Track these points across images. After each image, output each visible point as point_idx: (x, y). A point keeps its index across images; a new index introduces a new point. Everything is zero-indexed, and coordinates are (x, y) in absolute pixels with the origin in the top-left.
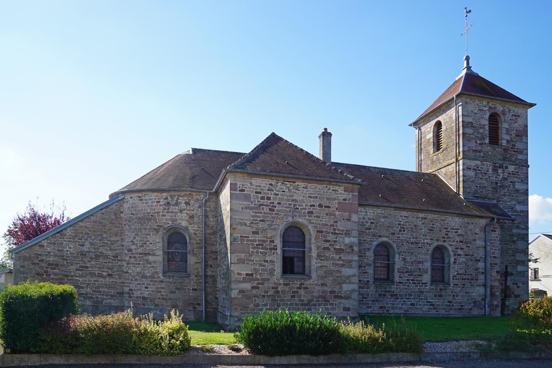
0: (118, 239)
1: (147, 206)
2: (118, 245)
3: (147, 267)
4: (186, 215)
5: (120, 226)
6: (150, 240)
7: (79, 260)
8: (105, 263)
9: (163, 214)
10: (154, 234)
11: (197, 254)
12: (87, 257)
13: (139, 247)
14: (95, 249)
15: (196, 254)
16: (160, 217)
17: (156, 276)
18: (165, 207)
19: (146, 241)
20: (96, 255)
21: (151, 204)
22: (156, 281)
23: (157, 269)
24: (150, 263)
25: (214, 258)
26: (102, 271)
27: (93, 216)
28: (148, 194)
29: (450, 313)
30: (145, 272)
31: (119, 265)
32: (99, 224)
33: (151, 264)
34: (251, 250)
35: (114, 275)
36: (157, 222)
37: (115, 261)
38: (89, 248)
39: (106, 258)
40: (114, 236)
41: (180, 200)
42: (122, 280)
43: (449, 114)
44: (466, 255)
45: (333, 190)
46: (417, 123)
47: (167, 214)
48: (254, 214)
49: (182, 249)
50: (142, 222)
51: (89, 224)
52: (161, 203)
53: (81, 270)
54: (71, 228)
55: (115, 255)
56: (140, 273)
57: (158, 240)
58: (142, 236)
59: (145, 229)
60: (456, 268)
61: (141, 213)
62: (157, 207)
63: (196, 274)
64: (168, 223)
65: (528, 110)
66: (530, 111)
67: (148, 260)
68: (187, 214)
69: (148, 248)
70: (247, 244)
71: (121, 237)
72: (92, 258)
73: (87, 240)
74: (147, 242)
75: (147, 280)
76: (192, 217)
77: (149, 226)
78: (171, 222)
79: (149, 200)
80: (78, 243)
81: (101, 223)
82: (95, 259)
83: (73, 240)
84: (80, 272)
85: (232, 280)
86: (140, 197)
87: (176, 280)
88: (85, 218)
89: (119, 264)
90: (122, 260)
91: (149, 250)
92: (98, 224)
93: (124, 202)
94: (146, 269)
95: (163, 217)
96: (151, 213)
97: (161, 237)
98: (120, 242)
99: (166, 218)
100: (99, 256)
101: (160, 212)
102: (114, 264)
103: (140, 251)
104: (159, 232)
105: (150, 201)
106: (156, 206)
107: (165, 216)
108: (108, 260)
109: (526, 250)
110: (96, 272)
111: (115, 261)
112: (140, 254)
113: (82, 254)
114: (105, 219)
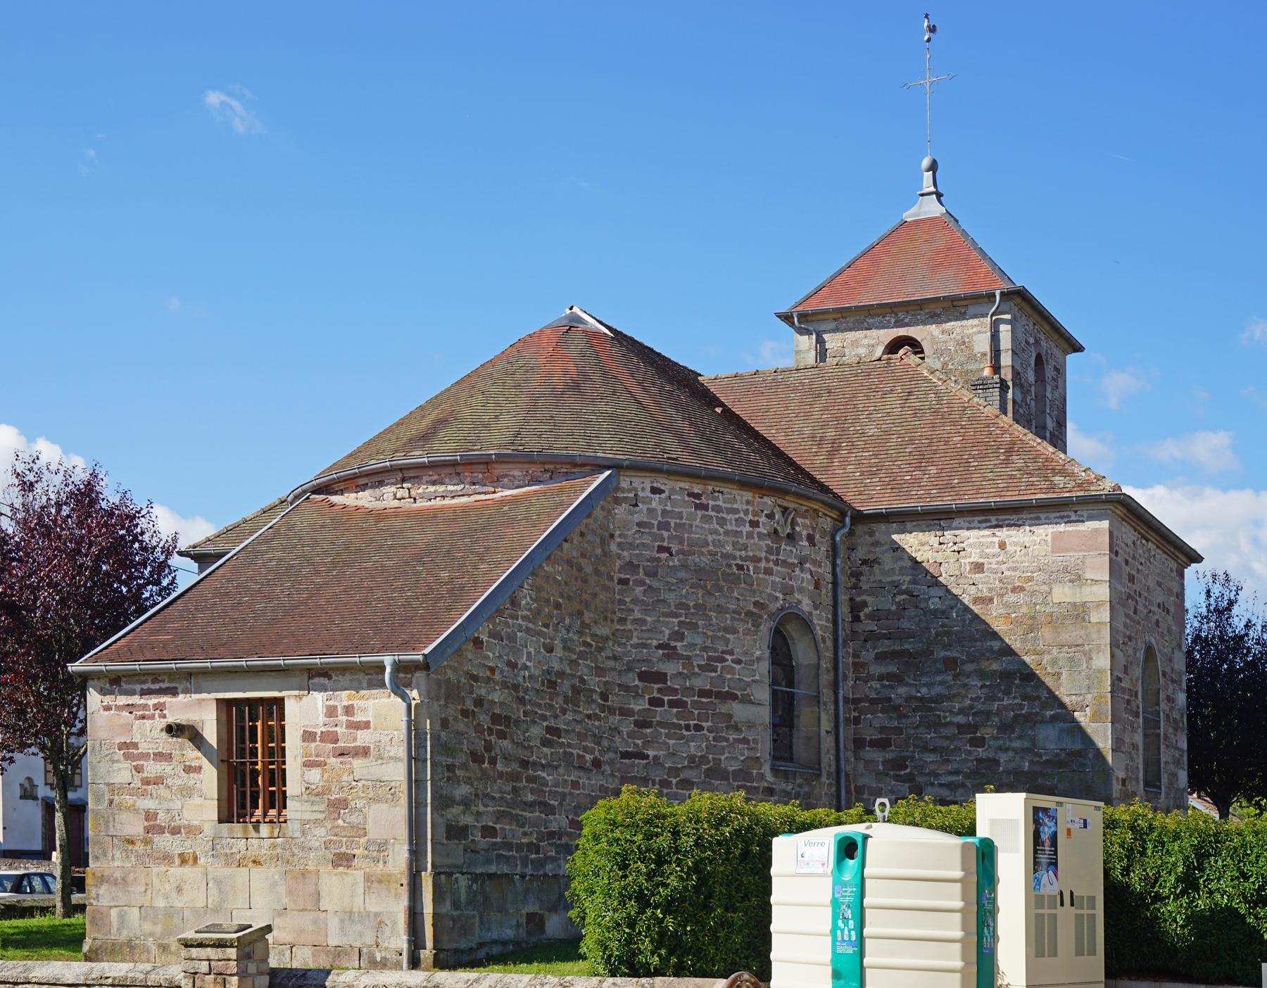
1: (722, 530)
3: (727, 740)
6: (735, 652)
10: (747, 632)
13: (696, 670)
16: (760, 576)
19: (723, 652)
24: (736, 728)
28: (725, 490)
30: (723, 758)
36: (754, 591)
43: (958, 330)
46: (809, 318)
52: (762, 530)
57: (758, 653)
58: (710, 633)
59: (720, 609)
61: (702, 554)
62: (752, 541)
67: (730, 716)
69: (729, 676)
77: (734, 601)
78: (781, 596)
86: (698, 496)
91: (732, 684)
94: (723, 748)
96: (735, 558)
97: (767, 644)
103: (701, 682)
105: (730, 516)
106: (750, 536)
112: (702, 693)
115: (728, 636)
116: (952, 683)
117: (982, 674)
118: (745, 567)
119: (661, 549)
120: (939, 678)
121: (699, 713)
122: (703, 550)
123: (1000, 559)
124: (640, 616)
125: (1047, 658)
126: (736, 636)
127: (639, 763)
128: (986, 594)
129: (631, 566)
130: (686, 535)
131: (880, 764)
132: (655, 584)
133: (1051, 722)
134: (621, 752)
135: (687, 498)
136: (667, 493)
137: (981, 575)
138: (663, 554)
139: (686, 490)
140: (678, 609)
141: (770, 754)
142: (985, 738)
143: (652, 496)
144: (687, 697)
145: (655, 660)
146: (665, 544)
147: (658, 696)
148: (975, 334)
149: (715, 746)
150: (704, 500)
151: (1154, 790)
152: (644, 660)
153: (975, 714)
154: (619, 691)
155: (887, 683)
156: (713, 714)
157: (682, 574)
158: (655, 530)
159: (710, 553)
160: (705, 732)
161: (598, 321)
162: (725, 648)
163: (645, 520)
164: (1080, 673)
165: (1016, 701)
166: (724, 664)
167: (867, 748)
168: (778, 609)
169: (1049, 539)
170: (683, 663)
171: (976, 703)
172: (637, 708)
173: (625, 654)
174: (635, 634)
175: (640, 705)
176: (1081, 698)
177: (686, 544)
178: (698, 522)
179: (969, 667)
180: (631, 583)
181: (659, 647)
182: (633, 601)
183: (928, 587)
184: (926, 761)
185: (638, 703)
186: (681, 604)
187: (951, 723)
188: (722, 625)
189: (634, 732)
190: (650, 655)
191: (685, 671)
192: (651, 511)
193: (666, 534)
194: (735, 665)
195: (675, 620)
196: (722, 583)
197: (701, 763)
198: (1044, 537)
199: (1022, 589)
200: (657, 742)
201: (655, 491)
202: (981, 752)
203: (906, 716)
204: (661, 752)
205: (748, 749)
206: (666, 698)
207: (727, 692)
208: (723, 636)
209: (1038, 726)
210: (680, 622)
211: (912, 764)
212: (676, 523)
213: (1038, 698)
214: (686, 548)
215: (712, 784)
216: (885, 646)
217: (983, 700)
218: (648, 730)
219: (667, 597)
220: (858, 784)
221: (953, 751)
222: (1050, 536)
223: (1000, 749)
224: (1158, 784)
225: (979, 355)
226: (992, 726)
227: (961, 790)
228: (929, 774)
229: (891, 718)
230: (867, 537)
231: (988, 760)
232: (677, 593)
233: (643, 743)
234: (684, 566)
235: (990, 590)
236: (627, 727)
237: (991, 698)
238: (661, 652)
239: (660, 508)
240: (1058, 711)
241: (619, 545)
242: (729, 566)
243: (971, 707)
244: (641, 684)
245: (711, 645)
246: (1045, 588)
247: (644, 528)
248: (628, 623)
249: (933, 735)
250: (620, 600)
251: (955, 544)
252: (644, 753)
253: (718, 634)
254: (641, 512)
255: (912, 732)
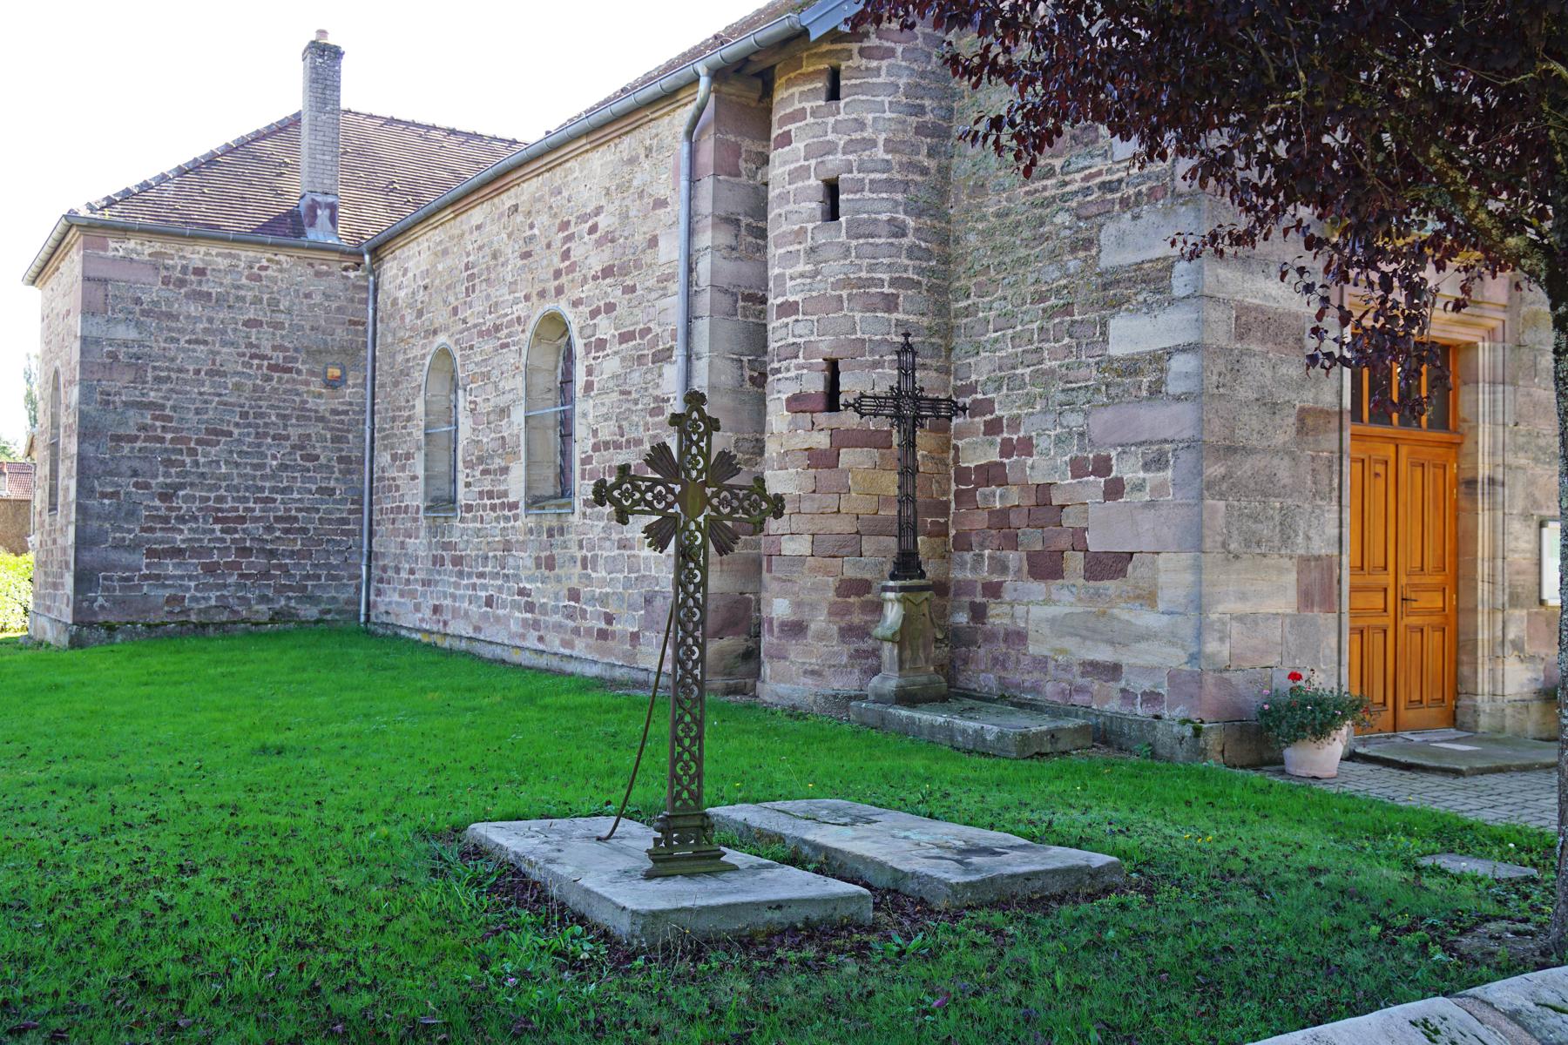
29: (575, 654)
44: (625, 338)
45: (873, 143)
60: (591, 417)
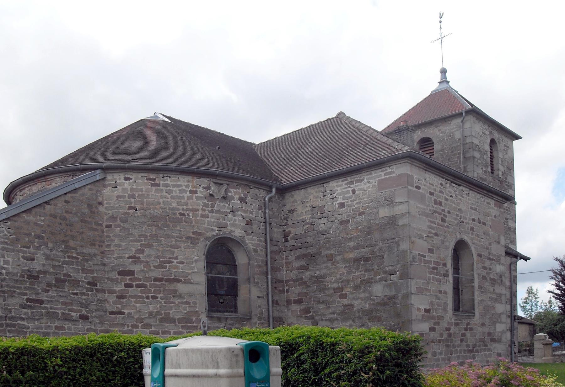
0: (96, 251)
1: (169, 196)
2: (96, 262)
3: (174, 303)
4: (241, 218)
5: (99, 228)
6: (179, 257)
7: (25, 288)
8: (74, 294)
9: (204, 213)
11: (258, 282)
12: (40, 282)
13: (152, 268)
14: (54, 267)
15: (258, 283)
16: (198, 218)
17: (194, 318)
18: (206, 201)
20: (57, 280)
21: (179, 195)
22: (194, 326)
23: (196, 307)
24: (180, 296)
25: (280, 291)
26: (69, 310)
27: (49, 204)
30: (171, 312)
31: (98, 300)
32: (61, 221)
33: (184, 298)
34: (428, 275)
35: (91, 317)
36: (193, 226)
37: (93, 291)
38: (43, 265)
39: (76, 285)
40: (89, 245)
41: (231, 192)
42: (106, 326)
47: (210, 214)
48: (429, 224)
49: (228, 274)
50: (160, 224)
51: (43, 218)
52: (199, 195)
53: (30, 307)
54: (8, 223)
55: (91, 280)
56: (159, 313)
57: (196, 258)
58: (161, 249)
59: (168, 236)
62: (192, 201)
63: (259, 315)
64: (213, 230)
65: (514, 142)
66: (515, 142)
67: (176, 291)
68: (243, 217)
70: (424, 265)
71: (101, 248)
72: (49, 285)
73: (38, 248)
74: (173, 260)
75: (176, 325)
76: (249, 223)
78: (217, 229)
79: (174, 186)
80: (21, 254)
81: (65, 219)
82: (55, 286)
83: (12, 247)
84: (29, 311)
85: (413, 318)
86: (153, 180)
87: (230, 324)
88: (34, 207)
89: (98, 297)
90: (104, 291)
92: (58, 220)
93: (105, 186)
94: (171, 307)
95: (204, 219)
96: (178, 210)
97: (203, 253)
98: (99, 257)
99: (208, 221)
100: (64, 281)
101: (197, 210)
102: (90, 297)
104: (198, 243)
106: (189, 198)
107: (207, 216)
108: (80, 289)
109: (516, 293)
110: (60, 312)
111: (93, 291)
112: (156, 280)
113: (30, 277)
114: (71, 213)
115: (173, 250)
116: (331, 267)
117: (345, 261)
118: (186, 214)
119: (130, 208)
120: (325, 265)
121: (154, 290)
122: (157, 207)
123: (353, 198)
124: (118, 243)
125: (376, 248)
126: (178, 249)
127: (120, 317)
128: (346, 218)
129: (113, 218)
130: (145, 200)
131: (298, 311)
132: (126, 225)
133: (379, 282)
134: (109, 312)
135: (146, 181)
136: (133, 179)
137: (343, 209)
138: (131, 211)
139: (145, 177)
140: (140, 238)
141: (206, 309)
142: (346, 294)
143: (125, 181)
144: (146, 282)
145: (127, 264)
146: (133, 205)
147: (129, 282)
148: (455, 131)
149: (166, 306)
150: (157, 181)
151: (467, 314)
152: (121, 265)
153: (342, 282)
154: (108, 281)
155: (301, 271)
156: (163, 290)
157: (143, 220)
158: (127, 199)
159: (161, 208)
160: (159, 299)
161: (163, 115)
162: (171, 256)
163: (121, 194)
164: (394, 253)
165: (362, 273)
166: (171, 264)
167: (292, 304)
168: (214, 235)
169: (376, 184)
170: (144, 265)
171: (342, 276)
172: (118, 289)
173: (111, 263)
174: (115, 252)
175: (119, 288)
176: (394, 267)
177: (145, 204)
178: (153, 193)
179: (339, 258)
180: (113, 226)
181: (130, 257)
182: (114, 236)
183: (319, 219)
184: (319, 308)
185: (118, 286)
186: (142, 235)
187: (331, 288)
188: (169, 244)
189: (116, 301)
190: (124, 262)
191: (145, 269)
192: (124, 190)
193: (133, 200)
194: (179, 265)
195: (139, 244)
196: (168, 222)
197: (156, 315)
198: (374, 184)
199: (363, 213)
200: (129, 306)
201: (126, 179)
202: (346, 302)
203: (309, 286)
204: (132, 311)
205: (189, 307)
206: (134, 283)
207: (173, 278)
208: (169, 250)
209: (373, 284)
210: (141, 244)
211: (313, 311)
212: (139, 194)
213: (373, 270)
214: (145, 206)
215: (164, 326)
216: (299, 252)
217: (345, 274)
218: (124, 300)
219: (133, 232)
220: (289, 322)
221: (332, 302)
222: (377, 183)
223: (354, 298)
224: (473, 311)
225: (457, 140)
226: (350, 287)
227: (336, 322)
228: (321, 315)
229: (303, 288)
230: (290, 198)
231: (349, 305)
232: (139, 229)
233: (121, 306)
234: (144, 216)
235: (348, 216)
236: (112, 299)
237: (349, 273)
238: (131, 260)
239: (129, 187)
240: (382, 275)
241: (106, 208)
242: (175, 214)
243: (340, 279)
244: (120, 277)
245: (161, 255)
246: (375, 210)
247: (121, 198)
248: (111, 247)
249: (322, 295)
250: (107, 236)
251: (331, 194)
252: (122, 312)
253: (167, 249)
254: (118, 190)
255: (313, 294)
